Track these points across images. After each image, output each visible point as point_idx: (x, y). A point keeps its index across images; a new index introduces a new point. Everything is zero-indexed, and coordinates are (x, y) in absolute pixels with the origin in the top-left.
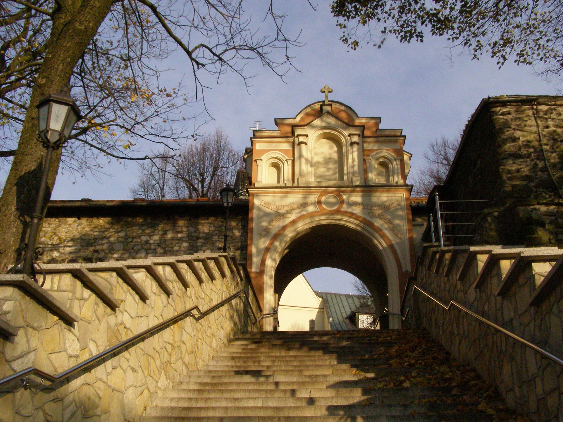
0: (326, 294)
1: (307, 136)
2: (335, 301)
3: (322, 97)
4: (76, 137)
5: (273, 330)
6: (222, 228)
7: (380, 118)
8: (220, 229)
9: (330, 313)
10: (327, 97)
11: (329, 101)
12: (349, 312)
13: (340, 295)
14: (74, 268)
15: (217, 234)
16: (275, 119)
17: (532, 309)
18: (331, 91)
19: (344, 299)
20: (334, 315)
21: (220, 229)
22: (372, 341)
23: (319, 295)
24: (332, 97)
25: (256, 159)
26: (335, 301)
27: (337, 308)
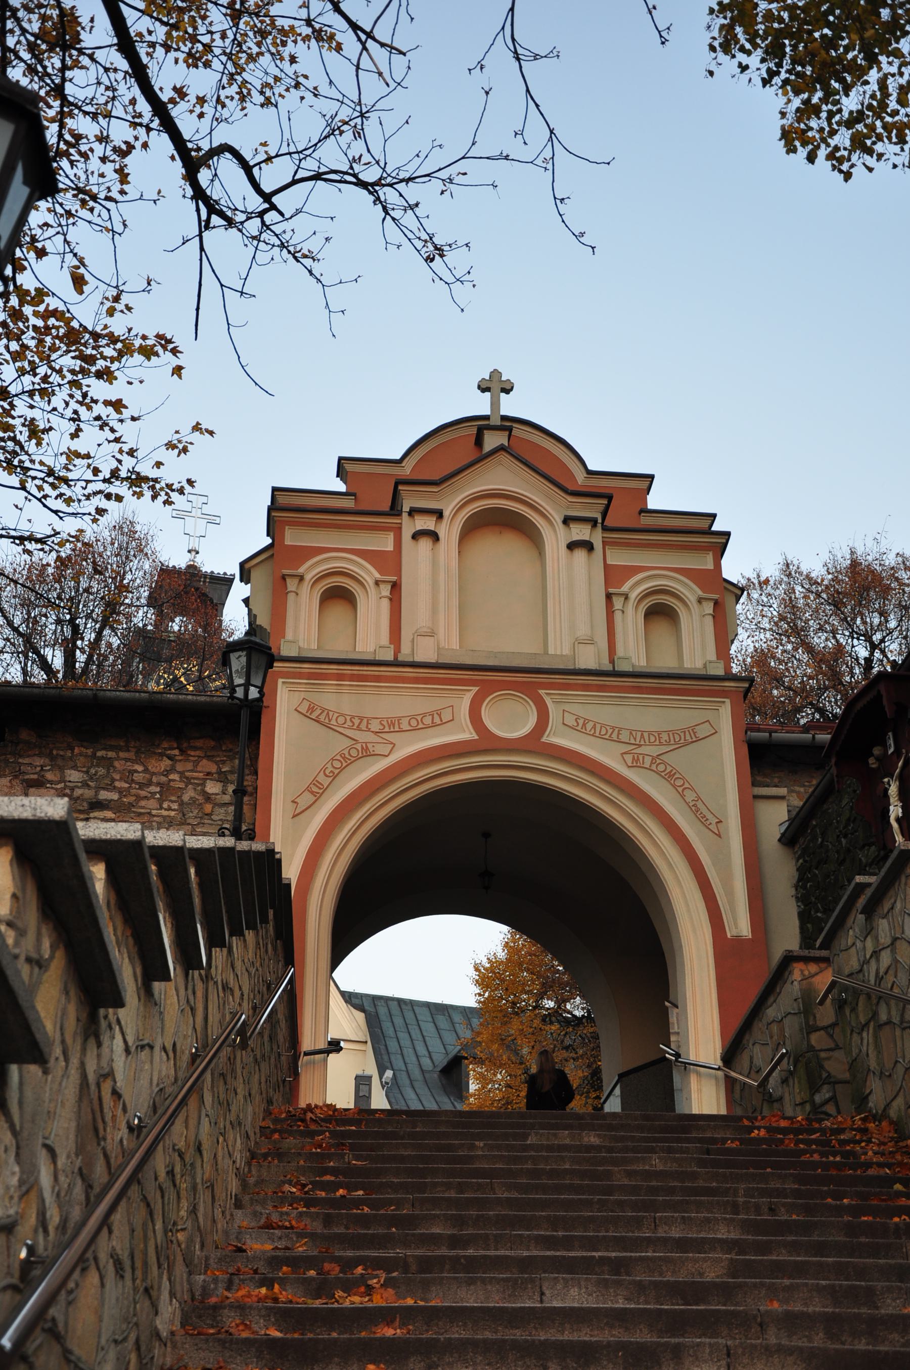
0: (375, 999)
1: (439, 514)
2: (398, 1021)
3: (481, 405)
4: (391, 185)
5: (682, 1108)
6: (172, 777)
7: (651, 477)
8: (163, 779)
9: (386, 1057)
10: (495, 404)
11: (504, 418)
12: (441, 1060)
13: (412, 1003)
14: (40, 814)
15: (154, 794)
16: (340, 459)
17: (785, 1086)
18: (508, 387)
19: (424, 1015)
20: (398, 1063)
21: (163, 779)
22: (871, 1172)
23: (354, 1001)
24: (510, 406)
25: (285, 572)
26: (398, 1021)
27: (406, 1042)
